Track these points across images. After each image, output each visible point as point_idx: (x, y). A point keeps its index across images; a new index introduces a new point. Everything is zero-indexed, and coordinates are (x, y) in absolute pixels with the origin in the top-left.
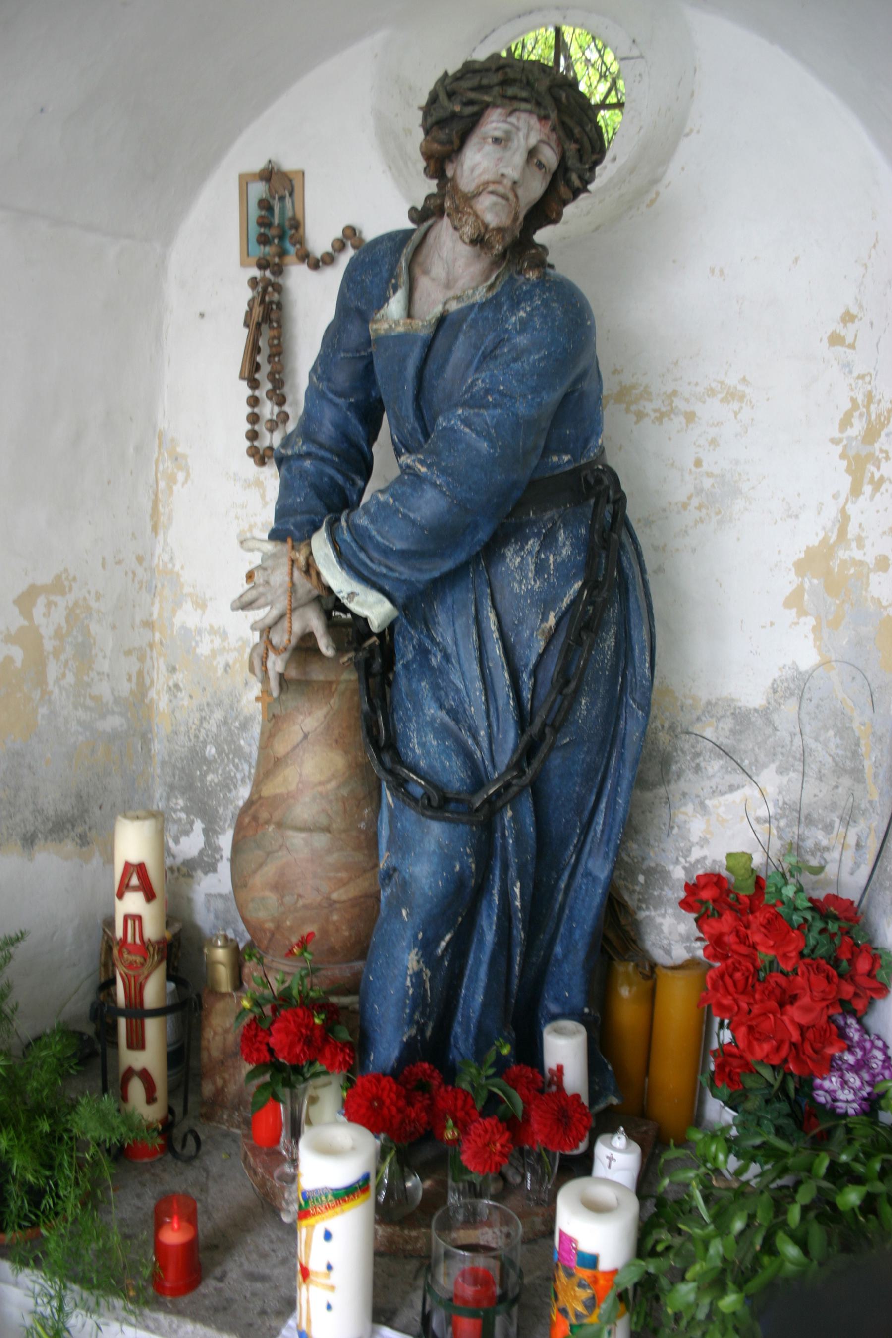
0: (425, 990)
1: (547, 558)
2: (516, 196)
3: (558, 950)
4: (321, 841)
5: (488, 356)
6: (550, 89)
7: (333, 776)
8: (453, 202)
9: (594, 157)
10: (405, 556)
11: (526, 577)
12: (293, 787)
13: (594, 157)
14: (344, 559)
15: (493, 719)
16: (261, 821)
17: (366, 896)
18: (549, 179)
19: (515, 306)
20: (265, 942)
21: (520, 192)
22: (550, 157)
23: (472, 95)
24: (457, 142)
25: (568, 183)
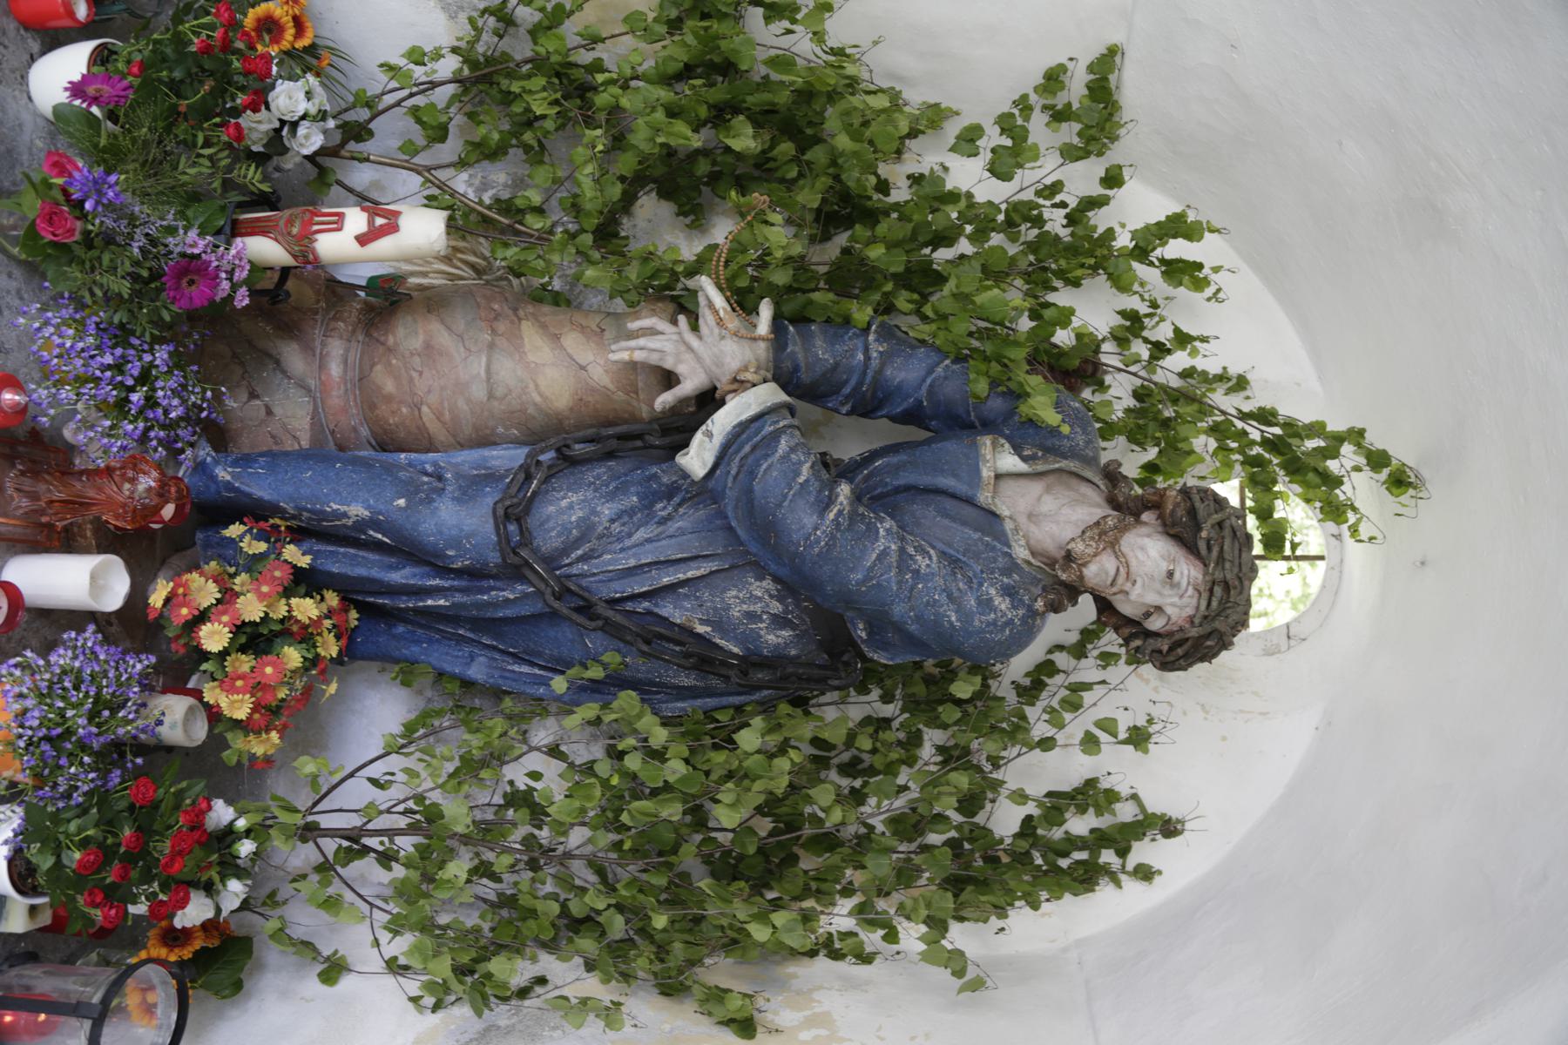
1: (762, 621)
2: (1115, 594)
3: (401, 629)
4: (479, 392)
5: (953, 563)
7: (545, 398)
12: (531, 357)
15: (600, 577)
16: (495, 324)
19: (1008, 592)
20: (375, 335)
22: (1155, 624)
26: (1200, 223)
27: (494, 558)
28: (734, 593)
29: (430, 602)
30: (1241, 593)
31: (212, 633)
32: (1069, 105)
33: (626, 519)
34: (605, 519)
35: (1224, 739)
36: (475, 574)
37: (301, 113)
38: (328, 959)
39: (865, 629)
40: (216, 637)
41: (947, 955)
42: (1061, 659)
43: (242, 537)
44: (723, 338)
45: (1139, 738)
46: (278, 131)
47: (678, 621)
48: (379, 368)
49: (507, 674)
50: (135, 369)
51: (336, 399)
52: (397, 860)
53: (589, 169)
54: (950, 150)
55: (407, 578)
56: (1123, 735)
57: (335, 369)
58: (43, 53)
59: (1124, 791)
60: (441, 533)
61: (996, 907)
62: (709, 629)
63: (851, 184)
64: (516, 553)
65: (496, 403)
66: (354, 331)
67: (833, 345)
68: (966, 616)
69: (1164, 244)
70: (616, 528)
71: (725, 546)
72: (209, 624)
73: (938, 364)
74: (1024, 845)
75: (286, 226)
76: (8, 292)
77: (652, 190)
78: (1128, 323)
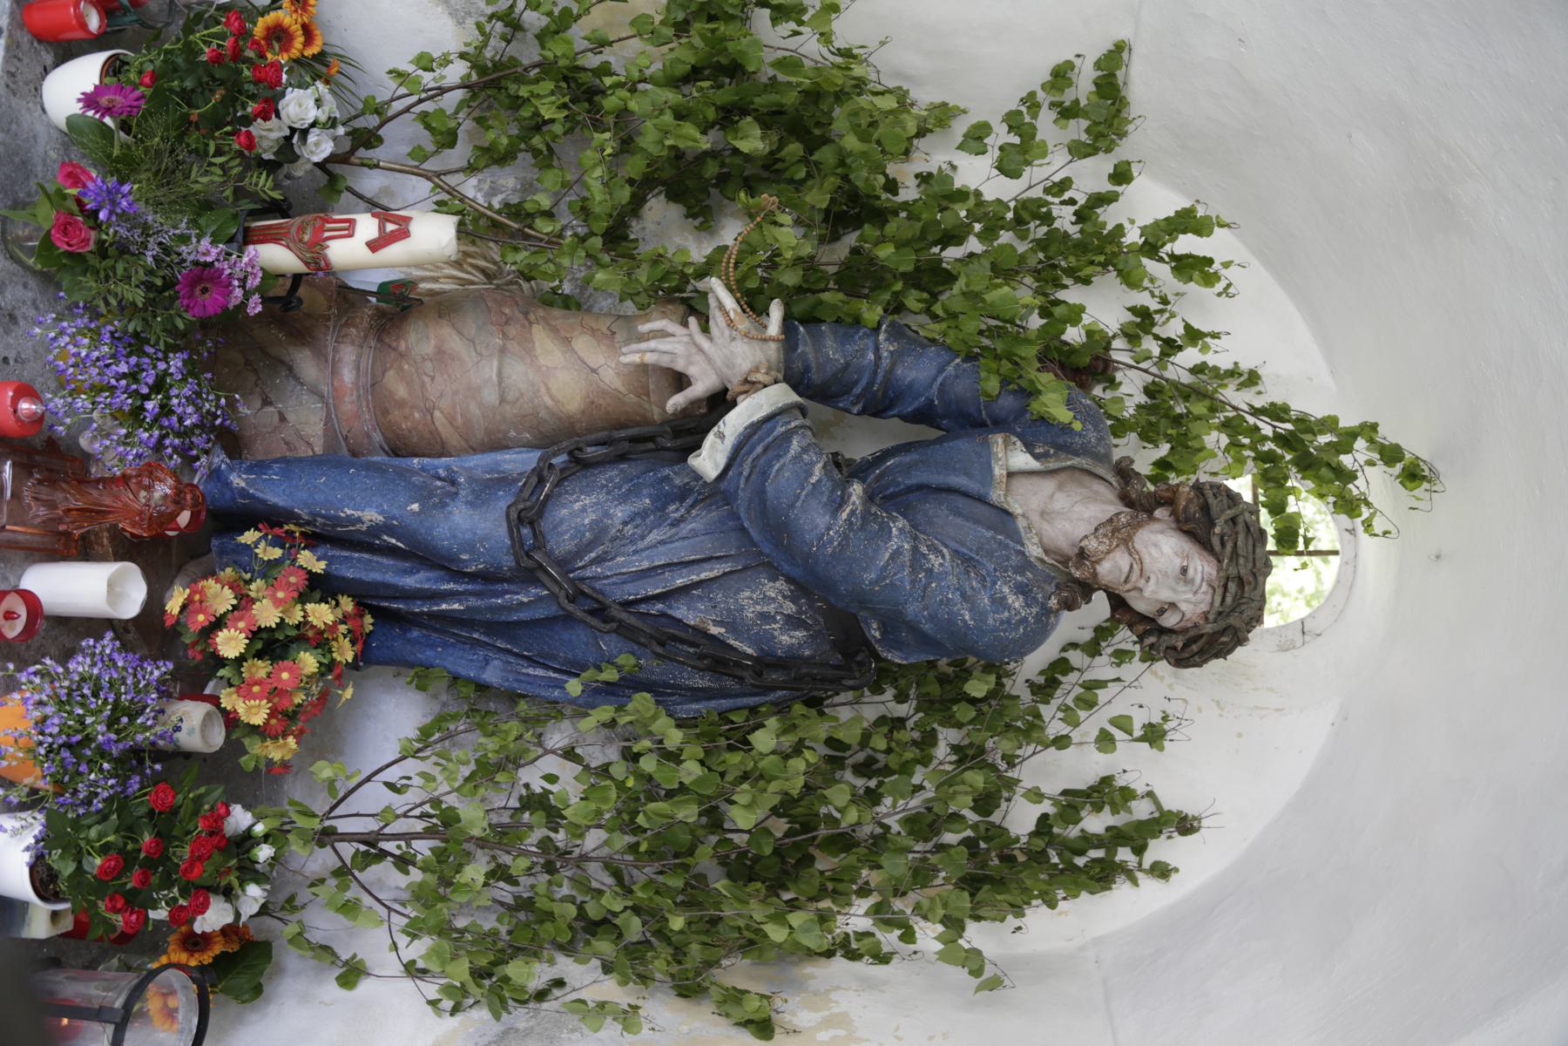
1: (776, 622)
2: (1128, 591)
3: (415, 633)
4: (490, 396)
5: (967, 562)
12: (542, 361)
14: (754, 429)
15: (614, 579)
16: (506, 328)
17: (443, 444)
19: (1022, 590)
21: (1133, 594)
22: (1169, 620)
26: (1208, 218)
27: (508, 562)
28: (747, 594)
29: (444, 606)
30: (1255, 588)
32: (1077, 101)
33: (639, 521)
34: (617, 522)
35: (1240, 735)
36: (489, 578)
37: (311, 121)
38: (346, 963)
39: (879, 628)
40: (233, 643)
41: (964, 954)
42: (1075, 657)
43: (257, 544)
45: (1154, 735)
46: (288, 139)
47: (692, 623)
48: (391, 373)
49: (522, 678)
51: (348, 405)
53: (598, 172)
54: (958, 148)
55: (421, 582)
56: (1138, 733)
57: (348, 375)
58: (57, 65)
59: (1140, 788)
61: (1012, 905)
62: (723, 630)
63: (860, 184)
65: (508, 407)
66: (366, 337)
67: (843, 345)
68: (979, 615)
69: (1173, 240)
70: (629, 530)
73: (948, 363)
75: (297, 233)
76: (24, 302)
77: (660, 192)
78: (1138, 320)
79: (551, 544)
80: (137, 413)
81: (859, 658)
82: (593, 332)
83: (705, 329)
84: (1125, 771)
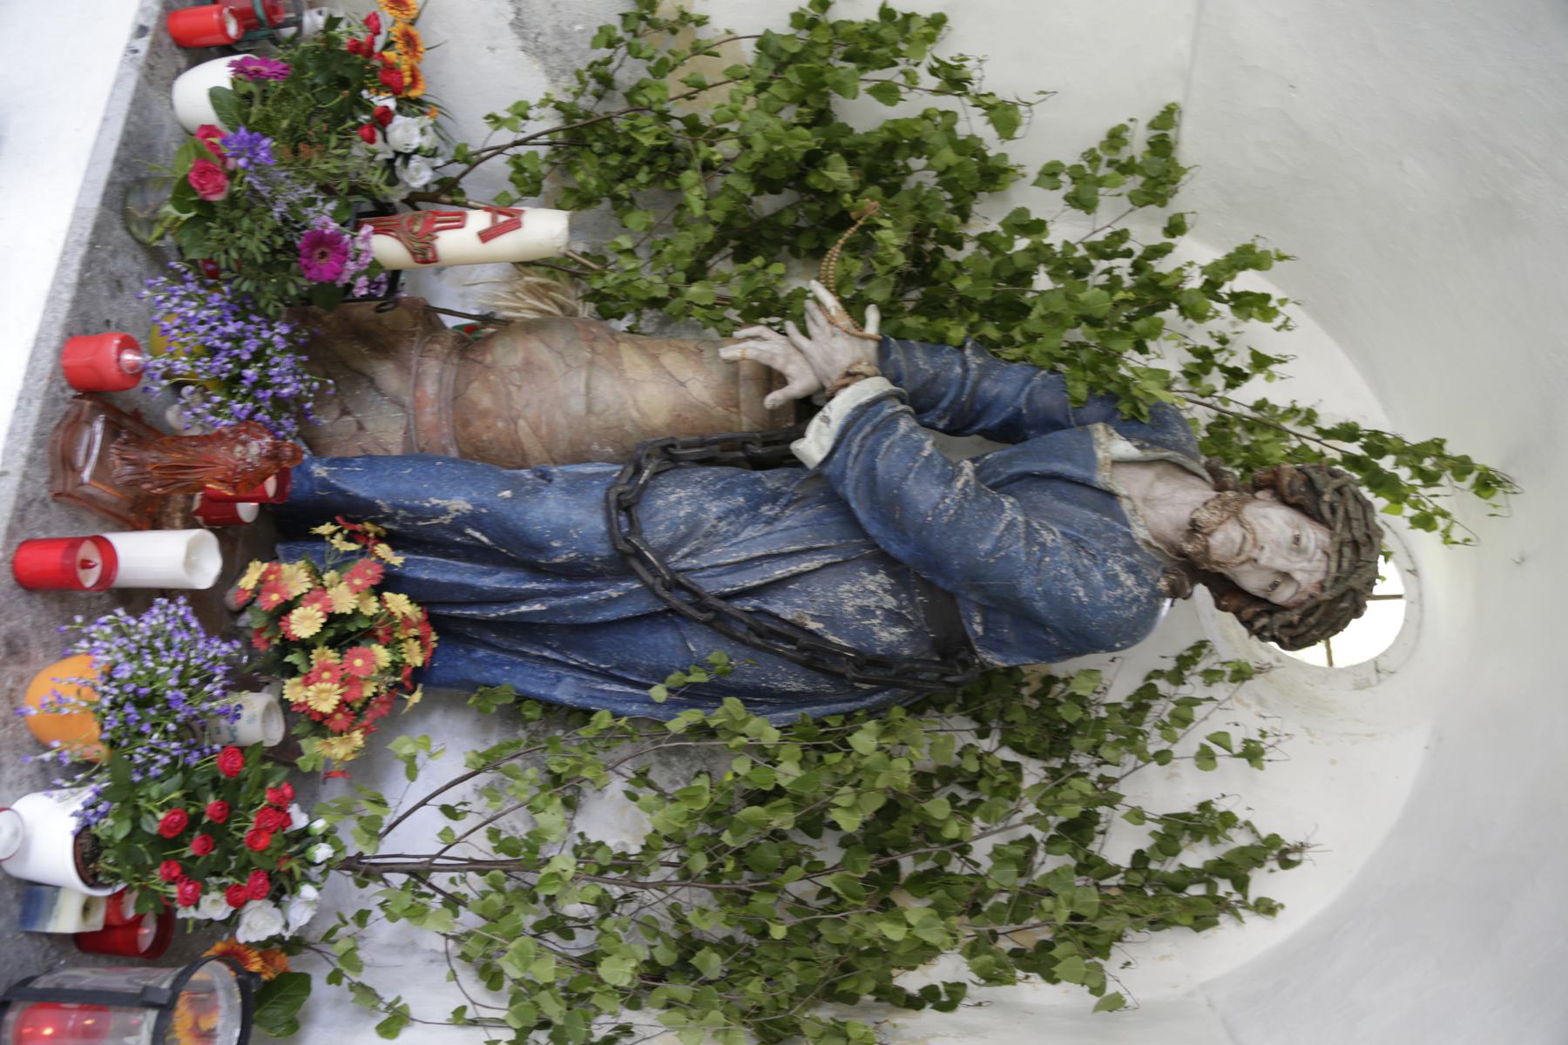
0: (429, 520)
1: (875, 617)
2: (1243, 563)
3: (481, 653)
4: (577, 405)
5: (1076, 542)
6: (1352, 590)
7: (643, 414)
8: (1232, 500)
9: (1286, 640)
10: (870, 471)
11: (857, 597)
12: (630, 374)
13: (1286, 640)
14: (862, 412)
17: (524, 456)
18: (1261, 595)
19: (1132, 569)
20: (472, 356)
21: (1247, 567)
22: (1284, 595)
23: (1341, 513)
24: (1292, 500)
25: (1258, 615)
26: (1267, 252)
27: (602, 550)
28: (847, 587)
29: (524, 608)
31: (304, 618)
32: (1132, 158)
33: (732, 518)
34: (712, 517)
35: (1333, 762)
36: (576, 572)
37: (415, 147)
38: (390, 1006)
40: (308, 623)
43: (332, 535)
44: (834, 335)
46: (390, 162)
48: (476, 385)
49: (597, 694)
50: (252, 345)
51: (429, 415)
52: (465, 905)
53: (697, 191)
55: (500, 582)
56: (1237, 749)
57: (430, 388)
59: (1242, 815)
60: (548, 521)
62: (821, 626)
64: (627, 541)
65: (593, 419)
66: (449, 354)
69: (1232, 278)
70: (723, 526)
71: (839, 539)
72: (301, 609)
73: (1034, 375)
74: (1138, 878)
77: (727, 256)
78: (1199, 361)
79: (647, 535)
80: (237, 379)
81: (961, 656)
82: (681, 350)
83: (805, 332)
84: (1224, 796)
